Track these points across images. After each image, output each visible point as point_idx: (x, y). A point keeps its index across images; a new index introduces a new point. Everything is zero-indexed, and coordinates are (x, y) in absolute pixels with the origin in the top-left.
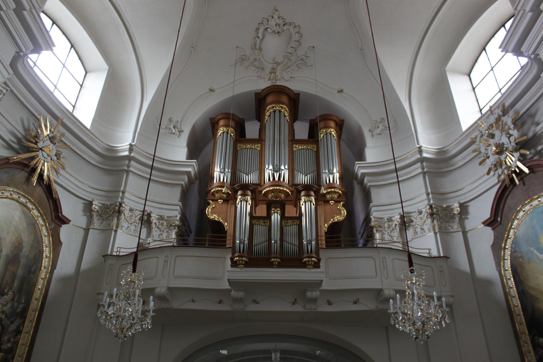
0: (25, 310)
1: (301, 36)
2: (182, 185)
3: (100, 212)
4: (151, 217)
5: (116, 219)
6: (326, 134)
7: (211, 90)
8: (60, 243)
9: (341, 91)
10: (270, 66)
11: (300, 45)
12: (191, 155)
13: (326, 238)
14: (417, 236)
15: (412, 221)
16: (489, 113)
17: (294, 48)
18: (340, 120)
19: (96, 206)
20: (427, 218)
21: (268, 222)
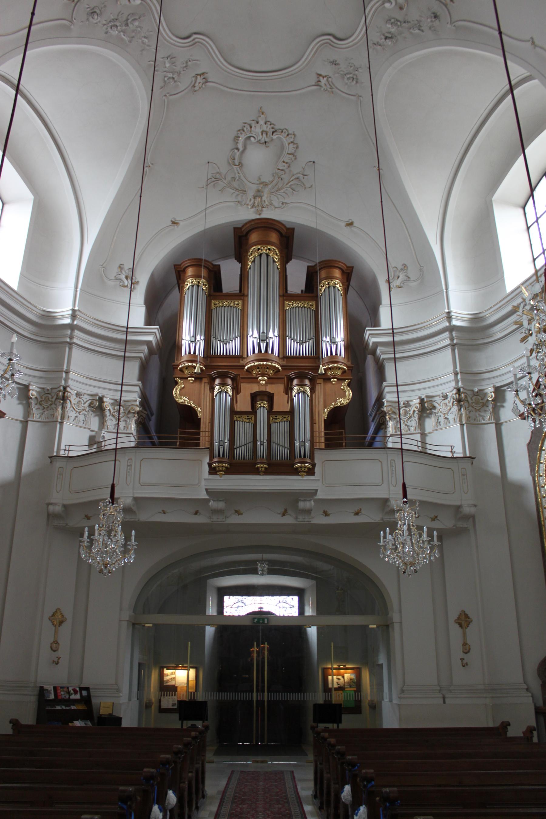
1: (297, 148)
2: (140, 358)
3: (39, 399)
4: (103, 402)
5: (60, 407)
6: (329, 287)
7: (174, 223)
9: (350, 224)
10: (255, 187)
11: (296, 159)
12: (150, 320)
13: (326, 434)
14: (439, 427)
15: (434, 407)
16: (535, 278)
17: (287, 163)
18: (348, 267)
19: (33, 393)
20: (453, 405)
21: (253, 418)
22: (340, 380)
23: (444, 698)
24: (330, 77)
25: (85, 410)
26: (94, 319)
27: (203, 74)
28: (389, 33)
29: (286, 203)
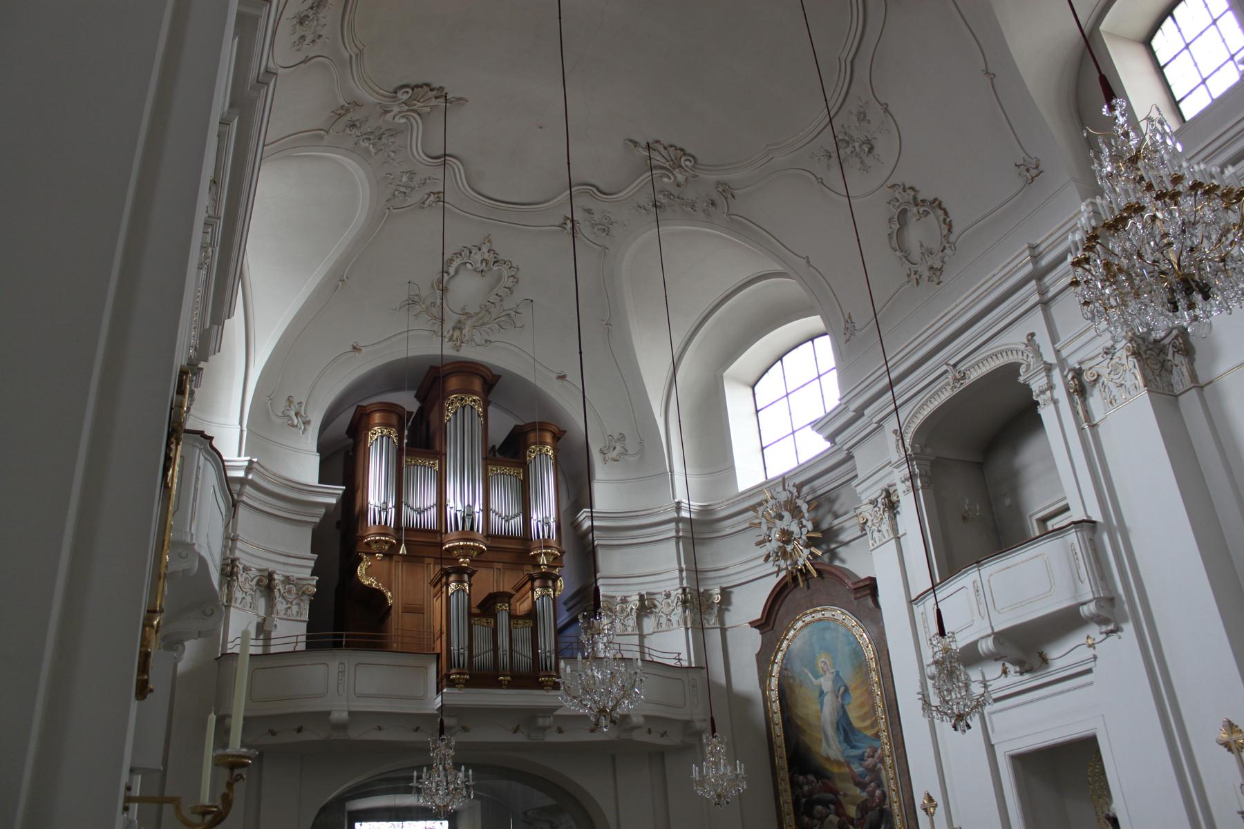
10: (456, 317)
15: (655, 606)
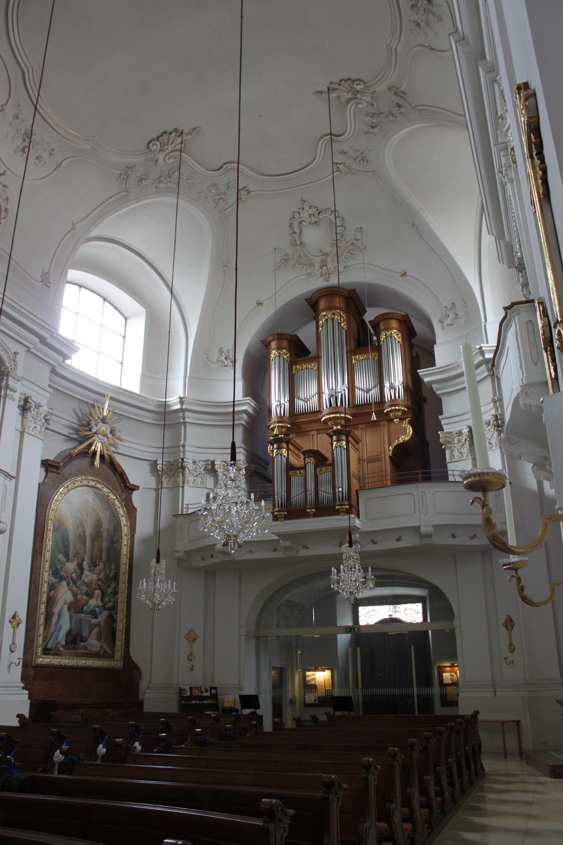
0: (117, 575)
1: (343, 220)
5: (181, 475)
7: (259, 304)
8: (135, 509)
9: (404, 274)
10: (319, 259)
11: (345, 229)
19: (159, 467)
22: (402, 419)
23: (495, 691)
24: (345, 163)
25: (201, 473)
26: (198, 401)
27: (244, 188)
28: (373, 123)
29: (348, 267)
